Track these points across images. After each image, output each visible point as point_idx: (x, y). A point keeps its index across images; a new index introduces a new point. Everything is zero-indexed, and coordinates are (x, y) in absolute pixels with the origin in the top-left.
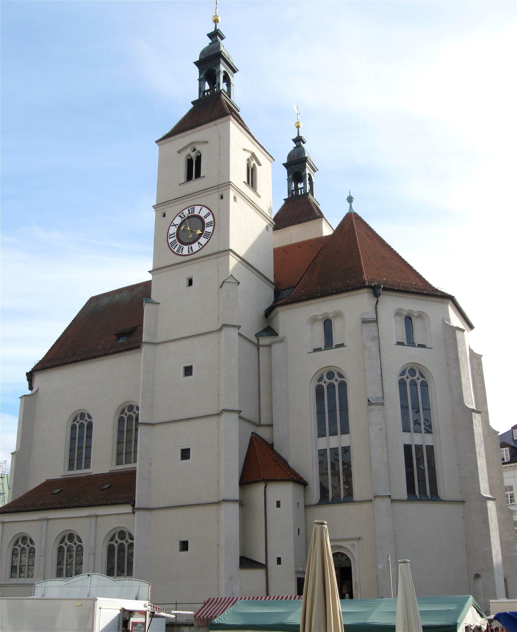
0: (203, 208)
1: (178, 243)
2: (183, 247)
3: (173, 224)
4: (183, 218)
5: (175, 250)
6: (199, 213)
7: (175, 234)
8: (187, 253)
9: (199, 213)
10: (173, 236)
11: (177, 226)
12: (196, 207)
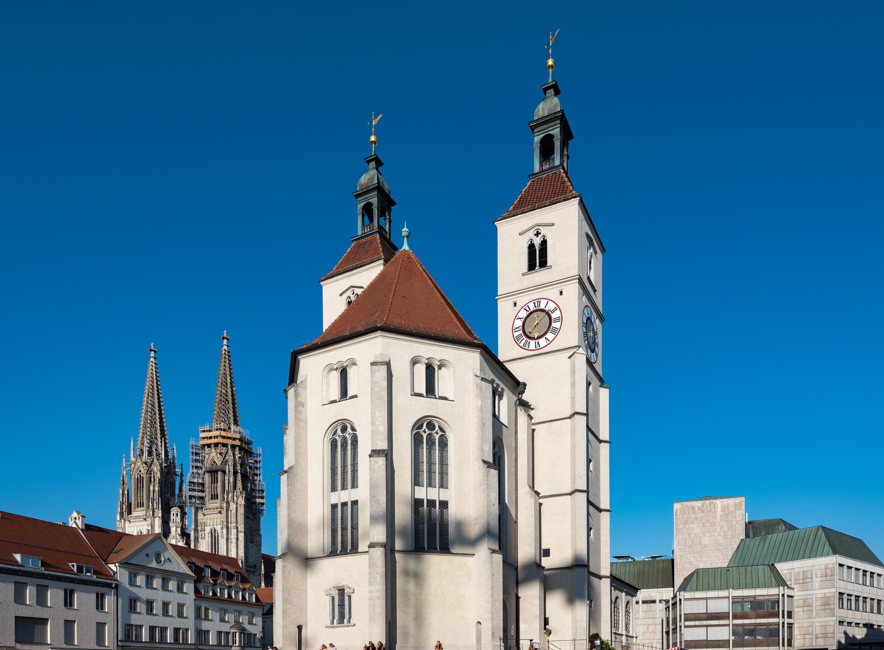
0: (550, 302)
1: (524, 337)
3: (517, 317)
4: (528, 311)
5: (522, 344)
6: (545, 307)
7: (521, 328)
8: (534, 348)
9: (545, 307)
10: (518, 329)
11: (522, 320)
12: (542, 300)
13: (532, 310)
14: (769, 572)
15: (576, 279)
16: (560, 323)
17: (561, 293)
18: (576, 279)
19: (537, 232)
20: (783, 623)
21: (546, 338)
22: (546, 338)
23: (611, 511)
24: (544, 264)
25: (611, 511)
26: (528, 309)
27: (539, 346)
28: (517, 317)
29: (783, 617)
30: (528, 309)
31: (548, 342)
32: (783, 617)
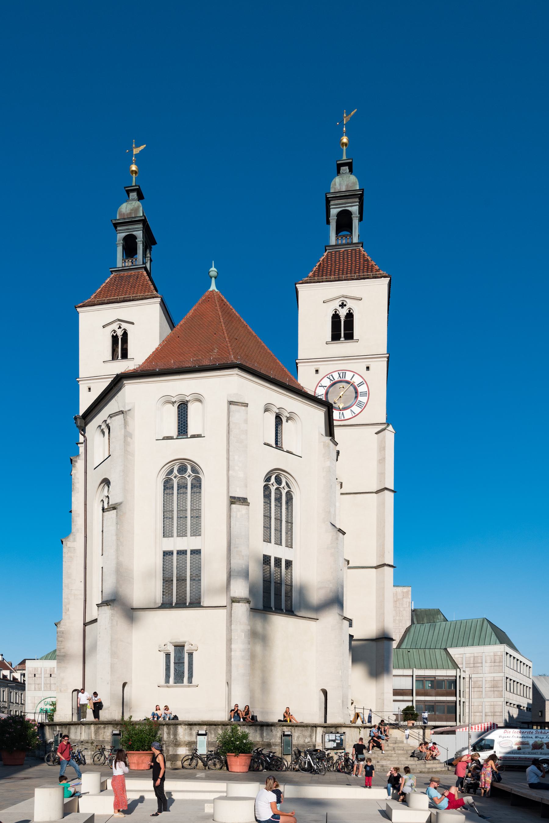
2: (343, 413)
3: (320, 385)
4: (332, 381)
13: (336, 379)
14: (445, 655)
15: (385, 357)
16: (367, 397)
17: (368, 368)
18: (385, 357)
19: (343, 303)
20: (460, 701)
21: (351, 410)
22: (351, 410)
23: (395, 567)
24: (349, 336)
25: (395, 567)
26: (331, 378)
27: (344, 418)
28: (320, 385)
29: (460, 696)
30: (331, 378)
31: (354, 415)
32: (460, 696)
